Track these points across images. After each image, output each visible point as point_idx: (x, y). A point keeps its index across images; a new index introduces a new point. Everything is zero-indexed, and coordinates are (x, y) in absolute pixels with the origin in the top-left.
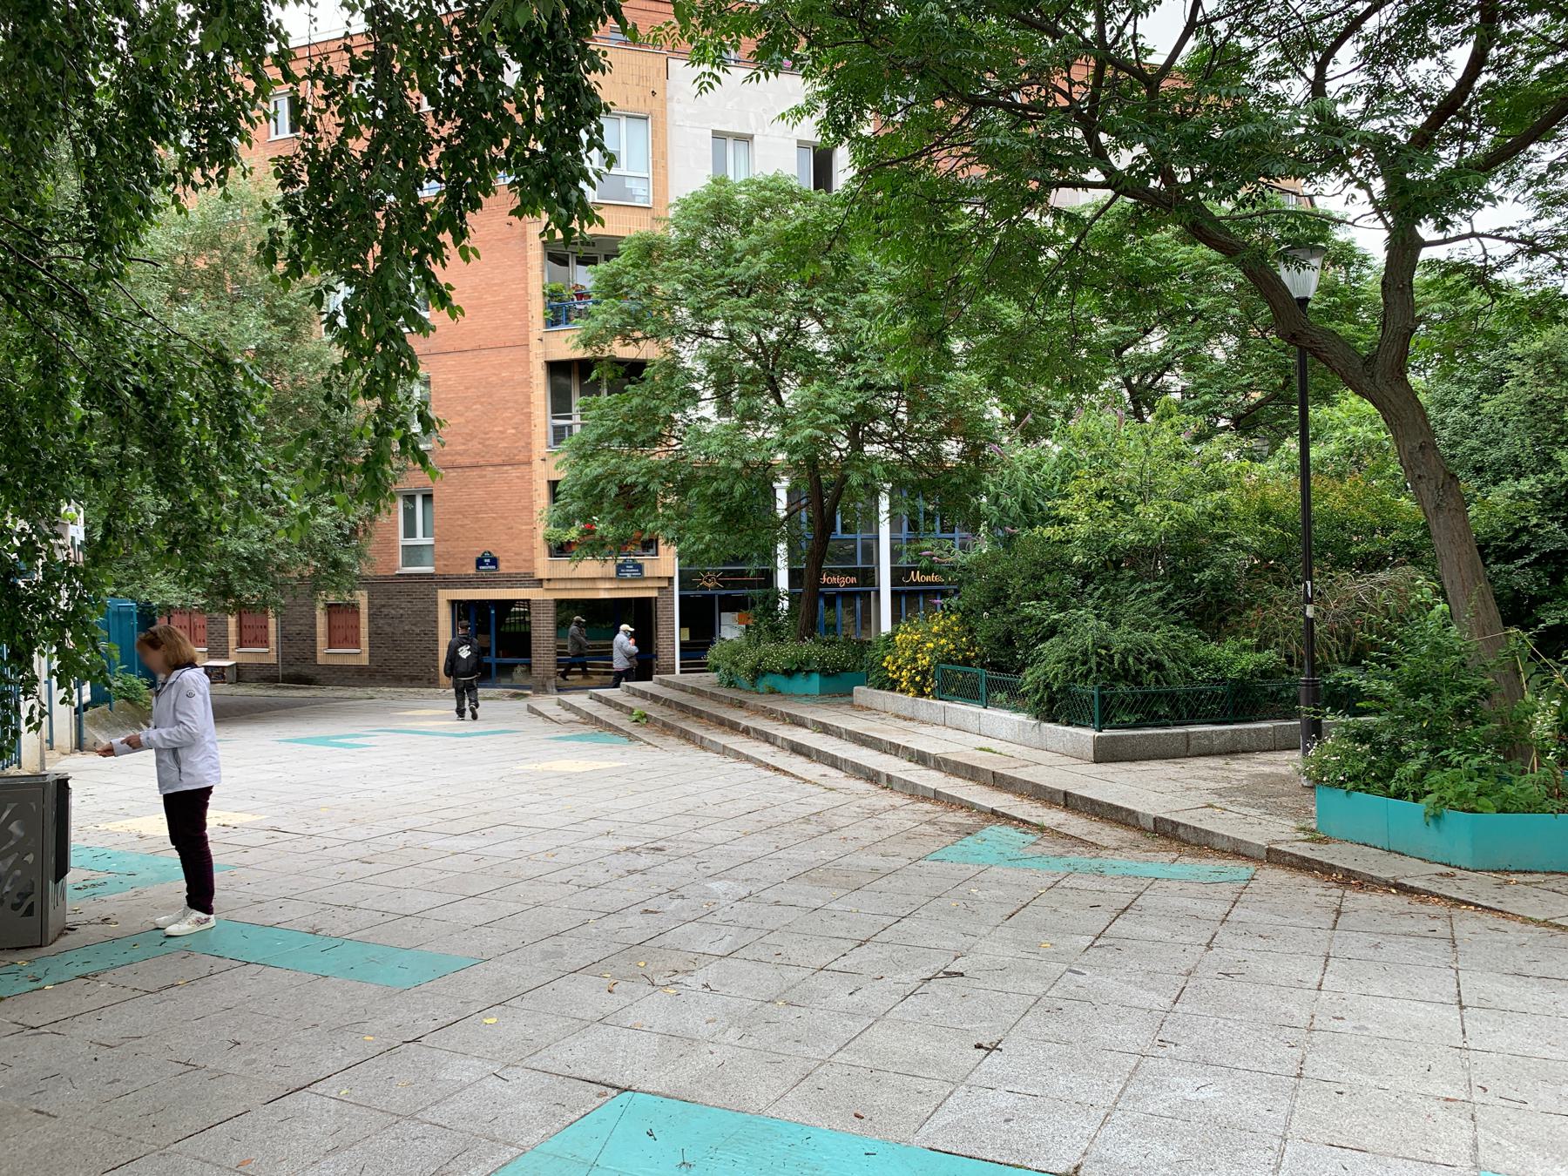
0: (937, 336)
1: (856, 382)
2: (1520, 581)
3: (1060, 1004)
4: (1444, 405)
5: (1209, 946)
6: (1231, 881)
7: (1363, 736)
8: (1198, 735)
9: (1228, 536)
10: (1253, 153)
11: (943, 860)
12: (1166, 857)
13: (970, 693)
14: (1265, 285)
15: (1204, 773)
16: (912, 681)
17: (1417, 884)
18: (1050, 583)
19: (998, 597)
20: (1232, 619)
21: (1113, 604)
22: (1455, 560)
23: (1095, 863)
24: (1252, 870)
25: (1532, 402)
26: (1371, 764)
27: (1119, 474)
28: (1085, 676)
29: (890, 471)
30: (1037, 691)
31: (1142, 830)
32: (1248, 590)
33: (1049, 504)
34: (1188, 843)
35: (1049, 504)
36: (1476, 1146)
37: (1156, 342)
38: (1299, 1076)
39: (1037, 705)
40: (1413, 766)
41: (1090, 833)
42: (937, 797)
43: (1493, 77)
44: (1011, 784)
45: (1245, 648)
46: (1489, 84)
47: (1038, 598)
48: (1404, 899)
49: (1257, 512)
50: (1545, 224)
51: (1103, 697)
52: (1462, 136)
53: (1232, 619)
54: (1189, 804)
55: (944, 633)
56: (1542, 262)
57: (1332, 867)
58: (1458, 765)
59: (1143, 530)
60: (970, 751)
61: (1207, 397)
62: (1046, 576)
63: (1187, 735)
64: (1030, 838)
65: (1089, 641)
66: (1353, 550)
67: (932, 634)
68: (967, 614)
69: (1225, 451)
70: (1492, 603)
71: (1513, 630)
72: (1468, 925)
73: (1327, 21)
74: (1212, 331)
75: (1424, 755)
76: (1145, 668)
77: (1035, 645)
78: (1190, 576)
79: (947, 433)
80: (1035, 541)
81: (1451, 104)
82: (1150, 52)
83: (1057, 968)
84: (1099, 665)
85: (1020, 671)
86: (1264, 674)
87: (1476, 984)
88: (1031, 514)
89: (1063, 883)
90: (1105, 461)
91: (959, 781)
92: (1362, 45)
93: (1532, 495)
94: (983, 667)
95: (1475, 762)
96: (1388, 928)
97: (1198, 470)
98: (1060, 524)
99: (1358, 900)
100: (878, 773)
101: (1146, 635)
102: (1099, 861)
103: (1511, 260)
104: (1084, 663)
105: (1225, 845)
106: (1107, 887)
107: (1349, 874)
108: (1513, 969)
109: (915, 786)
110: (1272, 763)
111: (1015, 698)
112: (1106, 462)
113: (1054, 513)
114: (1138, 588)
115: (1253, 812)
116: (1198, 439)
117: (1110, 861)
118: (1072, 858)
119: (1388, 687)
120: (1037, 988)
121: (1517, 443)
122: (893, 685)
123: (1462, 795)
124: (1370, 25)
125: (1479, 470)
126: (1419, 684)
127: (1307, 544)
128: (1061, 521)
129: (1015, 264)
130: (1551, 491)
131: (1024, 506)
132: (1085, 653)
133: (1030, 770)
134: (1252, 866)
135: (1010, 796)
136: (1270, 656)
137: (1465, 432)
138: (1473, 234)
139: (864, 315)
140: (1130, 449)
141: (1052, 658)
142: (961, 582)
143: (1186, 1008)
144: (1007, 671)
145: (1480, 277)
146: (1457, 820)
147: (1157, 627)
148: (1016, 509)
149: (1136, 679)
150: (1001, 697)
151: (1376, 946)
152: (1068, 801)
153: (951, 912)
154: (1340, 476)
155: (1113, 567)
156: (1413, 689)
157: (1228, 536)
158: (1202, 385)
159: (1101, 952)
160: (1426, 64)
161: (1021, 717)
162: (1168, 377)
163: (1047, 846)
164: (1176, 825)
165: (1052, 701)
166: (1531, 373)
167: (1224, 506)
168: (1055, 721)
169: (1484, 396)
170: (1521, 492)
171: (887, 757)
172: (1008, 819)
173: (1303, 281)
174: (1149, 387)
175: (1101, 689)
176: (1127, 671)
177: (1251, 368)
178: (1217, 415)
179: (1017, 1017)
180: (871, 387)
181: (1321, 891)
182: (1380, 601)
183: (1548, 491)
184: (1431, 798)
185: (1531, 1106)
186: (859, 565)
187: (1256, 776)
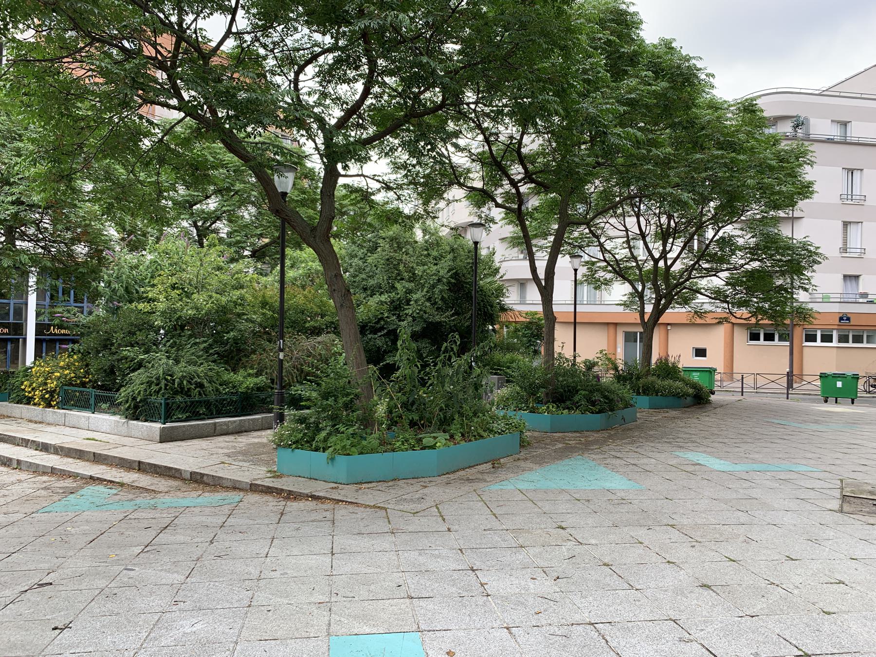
0: (67, 178)
1: (10, 199)
2: (379, 343)
3: (115, 591)
4: (352, 256)
5: (211, 542)
6: (229, 504)
7: (302, 420)
8: (221, 424)
9: (244, 314)
10: (257, 110)
11: (49, 512)
12: (194, 494)
13: (83, 404)
14: (266, 184)
15: (222, 445)
16: (42, 398)
17: (321, 494)
18: (140, 336)
19: (106, 344)
20: (244, 360)
21: (178, 350)
22: (349, 330)
23: (152, 502)
24: (241, 496)
25: (388, 260)
26: (305, 434)
27: (184, 275)
28: (157, 392)
29: (35, 260)
30: (127, 402)
31: (184, 480)
32: (253, 344)
33: (142, 289)
34: (208, 485)
35: (142, 289)
36: (330, 624)
37: (212, 204)
38: (249, 606)
39: (127, 410)
40: (323, 434)
41: (152, 484)
42: (53, 471)
43: (374, 101)
44: (105, 459)
45: (249, 375)
46: (372, 104)
47: (132, 346)
48: (315, 502)
49: (261, 302)
50: (393, 177)
51: (167, 404)
52: (359, 126)
53: (244, 360)
54: (212, 463)
55: (68, 367)
56: (391, 194)
57: (282, 490)
58: (343, 433)
59: (197, 309)
60: (79, 441)
61: (238, 238)
62: (138, 333)
63: (215, 424)
64: (114, 491)
65: (161, 372)
66: (307, 325)
67: (63, 366)
68: (85, 354)
69: (247, 269)
70: (362, 353)
71: (371, 366)
72: (342, 512)
73: (302, 52)
74: (243, 203)
75: (328, 428)
76: (193, 387)
77: (129, 374)
78: (222, 335)
79: (76, 240)
80: (132, 311)
81: (354, 110)
82: (210, 41)
83: (117, 568)
84: (166, 385)
85: (118, 390)
86: (259, 389)
87: (343, 541)
88: (130, 294)
89: (130, 516)
90: (178, 267)
91: (70, 460)
92: (317, 69)
93: (386, 303)
94: (94, 388)
95: (351, 431)
96: (304, 519)
97: (229, 277)
98: (148, 302)
99: (294, 506)
100: (10, 460)
101: (195, 368)
102: (155, 500)
103: (379, 190)
104: (157, 385)
105: (229, 484)
106: (157, 515)
107: (290, 493)
108: (357, 531)
109: (38, 465)
110: (260, 437)
111: (113, 407)
112: (178, 269)
113: (145, 295)
114: (192, 341)
115: (245, 464)
116: (233, 260)
117: (161, 500)
118: (139, 501)
119: (314, 394)
120: (102, 583)
121: (380, 278)
122: (29, 401)
123: (344, 447)
124: (321, 59)
125: (365, 289)
126: (329, 393)
127: (282, 321)
128: (150, 300)
129: (123, 142)
130: (394, 301)
131: (127, 290)
132: (158, 379)
133: (119, 450)
134: (242, 494)
135: (104, 467)
136: (262, 380)
137: (360, 270)
138: (362, 175)
139: (20, 156)
140: (187, 259)
141: (138, 382)
142: (82, 334)
143: (193, 580)
144: (110, 390)
145: (365, 196)
146: (341, 460)
147: (202, 364)
148: (122, 291)
149: (188, 393)
150: (104, 406)
151: (298, 529)
152: (141, 467)
153: (50, 545)
154: (303, 287)
155: (180, 327)
156: (326, 396)
157: (244, 314)
158: (236, 231)
159: (147, 555)
160: (345, 87)
161: (117, 418)
162: (218, 224)
163: (124, 495)
164: (202, 475)
165: (136, 407)
166: (387, 246)
167: (242, 298)
168: (137, 419)
169: (369, 254)
170: (381, 301)
171: (18, 448)
172: (100, 481)
173: (285, 182)
174: (207, 228)
175: (166, 399)
176: (182, 389)
177: (262, 225)
178: (243, 248)
179: (85, 604)
180: (22, 203)
181: (275, 504)
182: (318, 351)
183: (392, 302)
184: (331, 449)
185: (356, 599)
186: (11, 321)
187: (250, 444)
